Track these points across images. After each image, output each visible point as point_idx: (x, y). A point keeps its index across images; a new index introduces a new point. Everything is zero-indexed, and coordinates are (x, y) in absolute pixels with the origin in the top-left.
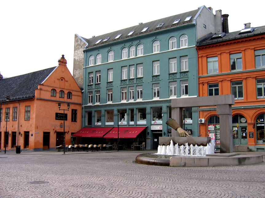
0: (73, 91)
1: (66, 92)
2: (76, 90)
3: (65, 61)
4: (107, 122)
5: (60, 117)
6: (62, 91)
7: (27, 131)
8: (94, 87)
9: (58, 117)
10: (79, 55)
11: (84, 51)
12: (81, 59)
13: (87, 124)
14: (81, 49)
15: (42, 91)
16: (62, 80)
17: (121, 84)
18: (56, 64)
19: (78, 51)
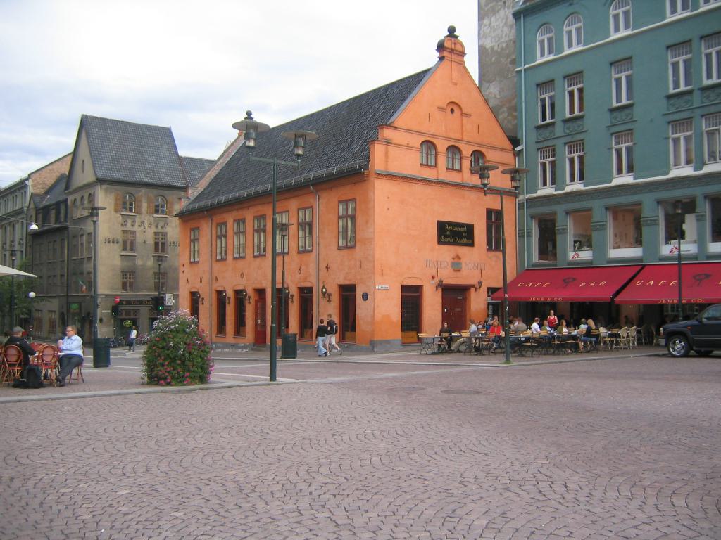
0: (487, 147)
1: (467, 151)
2: (497, 144)
3: (458, 48)
4: (614, 248)
5: (453, 234)
6: (454, 149)
7: (347, 282)
8: (559, 130)
9: (446, 236)
10: (498, 32)
11: (516, 15)
12: (504, 45)
13: (535, 258)
14: (502, 13)
15: (390, 148)
16: (452, 111)
17: (668, 109)
18: (432, 58)
19: (493, 19)
